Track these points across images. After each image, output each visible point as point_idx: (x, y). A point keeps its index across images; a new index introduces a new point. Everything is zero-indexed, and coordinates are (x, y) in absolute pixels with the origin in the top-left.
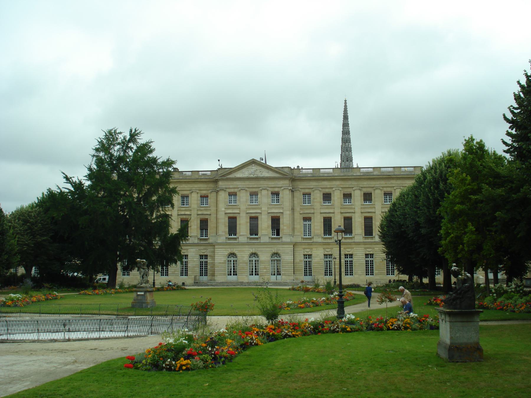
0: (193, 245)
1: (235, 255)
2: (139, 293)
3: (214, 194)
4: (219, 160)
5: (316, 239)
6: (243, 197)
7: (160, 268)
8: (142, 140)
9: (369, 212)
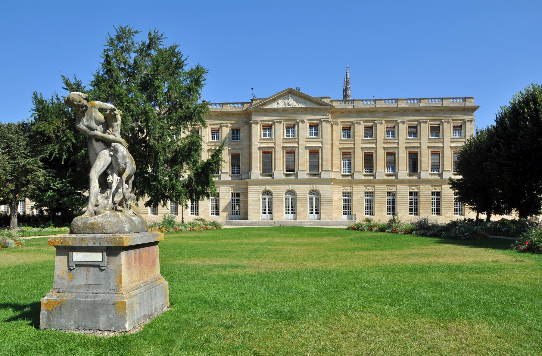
0: (226, 183)
1: (270, 192)
2: (77, 257)
3: (246, 128)
4: (252, 89)
5: (357, 176)
6: (280, 130)
7: (189, 203)
8: (164, 45)
9: (414, 147)
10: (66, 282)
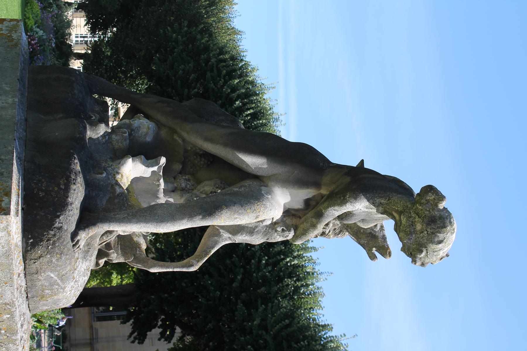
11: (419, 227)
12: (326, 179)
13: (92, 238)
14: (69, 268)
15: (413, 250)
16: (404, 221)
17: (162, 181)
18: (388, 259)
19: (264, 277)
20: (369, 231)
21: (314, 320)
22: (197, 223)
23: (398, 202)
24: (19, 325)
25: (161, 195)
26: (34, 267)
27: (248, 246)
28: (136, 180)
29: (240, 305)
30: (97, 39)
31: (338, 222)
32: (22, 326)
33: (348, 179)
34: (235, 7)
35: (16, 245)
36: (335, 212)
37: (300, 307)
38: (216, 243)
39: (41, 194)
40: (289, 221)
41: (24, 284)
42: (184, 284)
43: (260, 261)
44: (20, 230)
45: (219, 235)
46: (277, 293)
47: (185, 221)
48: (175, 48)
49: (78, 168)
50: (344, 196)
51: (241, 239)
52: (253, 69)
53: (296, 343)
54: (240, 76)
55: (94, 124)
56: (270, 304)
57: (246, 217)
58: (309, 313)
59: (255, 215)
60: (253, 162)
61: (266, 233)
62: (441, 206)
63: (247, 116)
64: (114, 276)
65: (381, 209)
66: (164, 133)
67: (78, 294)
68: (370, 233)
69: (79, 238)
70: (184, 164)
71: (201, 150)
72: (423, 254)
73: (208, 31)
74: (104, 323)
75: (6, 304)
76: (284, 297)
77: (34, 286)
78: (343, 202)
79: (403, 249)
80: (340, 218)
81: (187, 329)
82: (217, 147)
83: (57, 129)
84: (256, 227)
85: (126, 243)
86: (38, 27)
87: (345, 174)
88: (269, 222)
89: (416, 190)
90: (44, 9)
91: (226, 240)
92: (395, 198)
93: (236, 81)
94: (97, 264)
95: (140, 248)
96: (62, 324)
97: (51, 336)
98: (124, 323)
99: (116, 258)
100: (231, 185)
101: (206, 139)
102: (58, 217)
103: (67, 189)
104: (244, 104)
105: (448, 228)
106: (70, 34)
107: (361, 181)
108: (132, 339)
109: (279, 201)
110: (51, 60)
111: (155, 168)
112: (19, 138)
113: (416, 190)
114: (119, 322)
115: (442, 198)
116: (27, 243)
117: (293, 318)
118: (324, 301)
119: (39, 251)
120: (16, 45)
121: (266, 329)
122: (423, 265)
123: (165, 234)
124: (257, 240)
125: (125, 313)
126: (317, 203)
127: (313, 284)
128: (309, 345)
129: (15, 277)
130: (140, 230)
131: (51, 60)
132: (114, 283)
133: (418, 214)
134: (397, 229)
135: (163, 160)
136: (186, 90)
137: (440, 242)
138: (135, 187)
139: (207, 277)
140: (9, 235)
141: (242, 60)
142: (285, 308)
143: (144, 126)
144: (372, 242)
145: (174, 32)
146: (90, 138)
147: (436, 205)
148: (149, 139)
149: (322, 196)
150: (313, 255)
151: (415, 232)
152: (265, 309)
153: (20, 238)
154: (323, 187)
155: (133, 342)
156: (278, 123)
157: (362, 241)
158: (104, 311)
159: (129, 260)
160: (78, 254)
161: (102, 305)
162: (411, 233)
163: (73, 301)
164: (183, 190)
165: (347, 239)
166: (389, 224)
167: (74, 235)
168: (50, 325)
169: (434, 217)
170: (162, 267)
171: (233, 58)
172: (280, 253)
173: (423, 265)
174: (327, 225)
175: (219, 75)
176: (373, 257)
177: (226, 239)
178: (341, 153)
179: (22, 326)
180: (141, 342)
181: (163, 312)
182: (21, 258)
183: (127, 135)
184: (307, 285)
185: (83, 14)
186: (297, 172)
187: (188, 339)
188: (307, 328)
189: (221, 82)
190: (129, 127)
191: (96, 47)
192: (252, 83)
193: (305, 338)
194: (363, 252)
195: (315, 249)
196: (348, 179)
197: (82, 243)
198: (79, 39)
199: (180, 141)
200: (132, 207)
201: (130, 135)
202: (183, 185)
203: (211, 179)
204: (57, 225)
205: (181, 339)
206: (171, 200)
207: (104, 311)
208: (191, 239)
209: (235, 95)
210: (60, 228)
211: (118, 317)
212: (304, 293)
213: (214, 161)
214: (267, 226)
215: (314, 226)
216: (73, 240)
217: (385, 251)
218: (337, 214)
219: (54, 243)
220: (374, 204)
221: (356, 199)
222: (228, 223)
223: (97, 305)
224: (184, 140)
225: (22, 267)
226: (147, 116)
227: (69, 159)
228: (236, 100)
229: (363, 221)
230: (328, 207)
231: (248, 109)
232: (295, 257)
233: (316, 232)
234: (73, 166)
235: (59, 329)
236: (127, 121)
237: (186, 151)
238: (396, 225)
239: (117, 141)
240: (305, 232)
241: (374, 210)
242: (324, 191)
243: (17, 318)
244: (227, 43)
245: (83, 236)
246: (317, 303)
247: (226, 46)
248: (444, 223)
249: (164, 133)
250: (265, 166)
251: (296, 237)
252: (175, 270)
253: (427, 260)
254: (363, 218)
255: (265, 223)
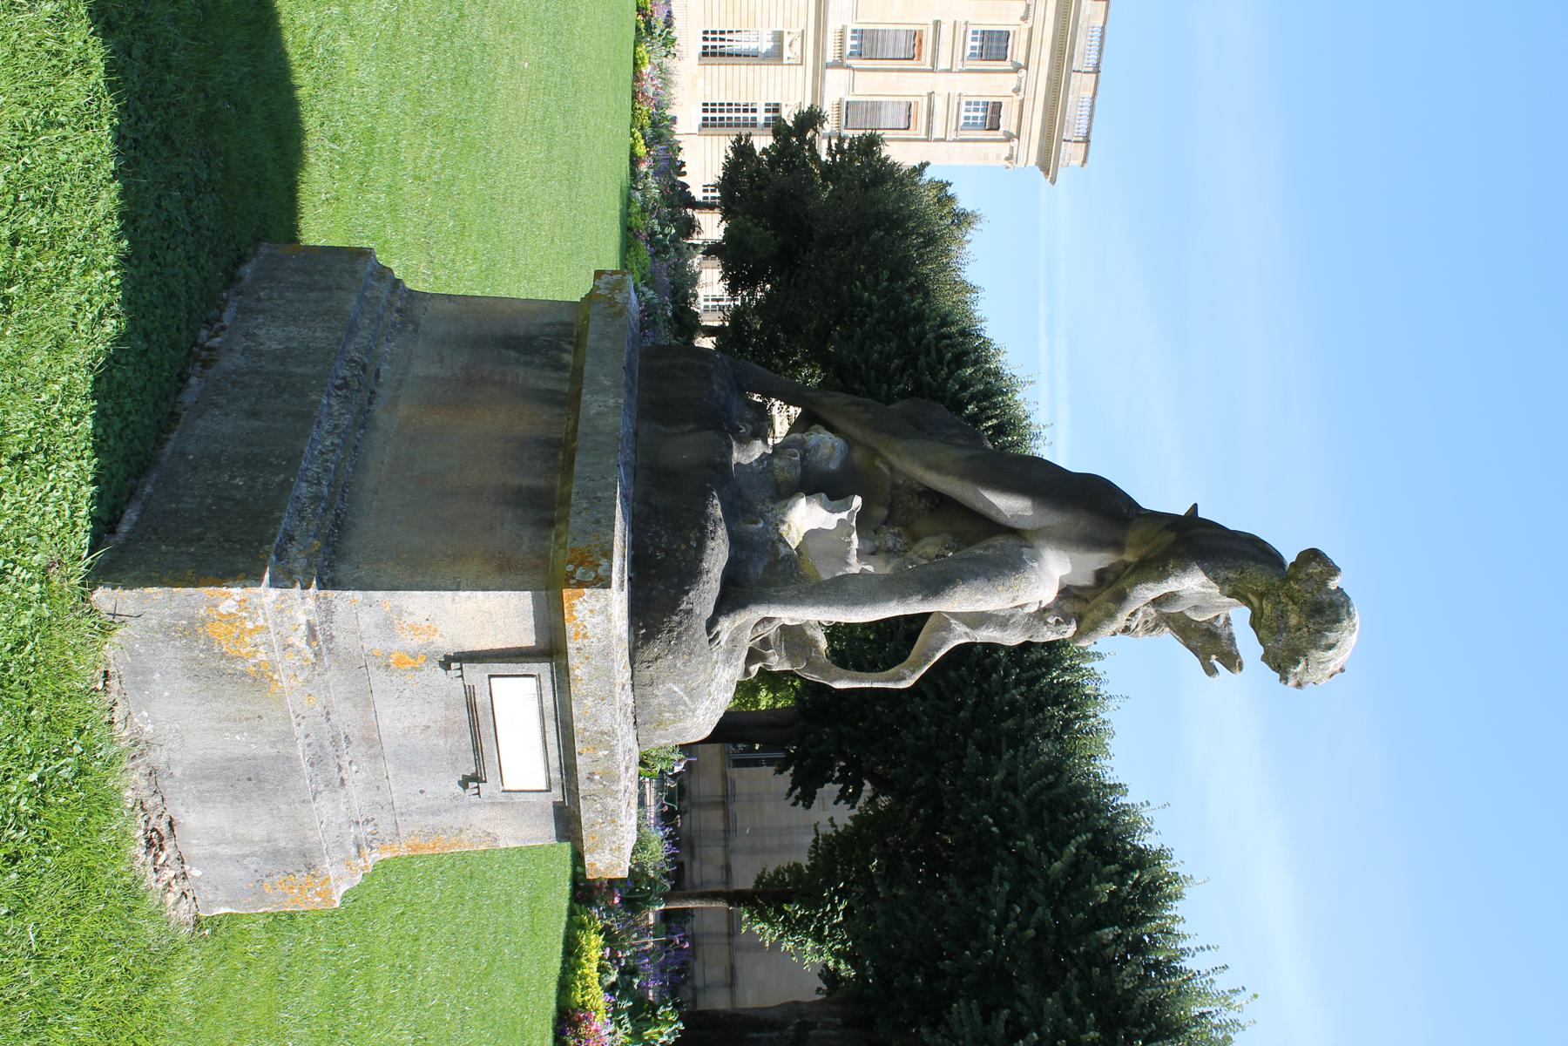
10: (374, 643)
11: (1293, 620)
12: (1133, 536)
13: (740, 629)
14: (702, 677)
15: (1282, 660)
16: (1267, 608)
17: (854, 536)
18: (1238, 675)
19: (1013, 702)
20: (1205, 626)
21: (1096, 776)
22: (914, 607)
23: (1259, 577)
24: (622, 769)
25: (853, 559)
26: (646, 674)
27: (991, 647)
28: (811, 534)
29: (971, 748)
30: (738, 303)
31: (1152, 610)
32: (627, 768)
33: (1171, 537)
34: (968, 247)
35: (620, 639)
36: (1149, 591)
37: (1072, 754)
38: (944, 642)
39: (660, 555)
40: (1068, 607)
41: (630, 701)
42: (879, 709)
43: (1007, 674)
44: (625, 614)
45: (947, 628)
46: (1033, 729)
47: (893, 604)
48: (866, 316)
49: (719, 513)
50: (1165, 566)
51: (985, 635)
52: (998, 351)
53: (1066, 814)
54: (976, 362)
55: (745, 441)
56: (1022, 748)
57: (996, 599)
58: (1088, 764)
59: (1011, 596)
60: (1009, 506)
61: (1028, 627)
62: (1333, 584)
63: (987, 429)
64: (763, 693)
65: (1227, 588)
66: (858, 456)
67: (716, 720)
68: (1208, 630)
69: (719, 628)
70: (891, 508)
71: (920, 484)
72: (1301, 666)
73: (922, 287)
74: (746, 770)
75: (602, 733)
76: (1046, 736)
77: (646, 705)
78: (1162, 576)
79: (1265, 658)
80: (1156, 602)
81: (881, 786)
82: (948, 479)
83: (685, 448)
84: (1012, 616)
85: (794, 638)
86: (646, 285)
87: (1168, 528)
88: (1033, 609)
89: (1290, 557)
90: (655, 254)
91: (960, 637)
92: (1253, 570)
93: (969, 371)
94: (747, 672)
95: (817, 647)
96: (677, 769)
97: (660, 787)
98: (780, 771)
99: (778, 662)
100: (969, 544)
101: (930, 467)
102: (687, 593)
103: (701, 548)
104: (982, 410)
105: (1345, 623)
106: (696, 296)
107: (1193, 540)
108: (792, 799)
109: (1053, 571)
110: (666, 337)
111: (844, 515)
112: (625, 464)
113: (1290, 557)
114: (772, 769)
115: (1334, 570)
116: (636, 635)
117: (1062, 773)
118: (1113, 745)
119: (655, 649)
120: (620, 313)
121: (1014, 789)
122: (1299, 685)
123: (847, 625)
124: (1012, 638)
125: (782, 755)
126: (1118, 577)
127: (1095, 716)
128: (1087, 817)
129: (618, 690)
130: (815, 617)
131: (666, 337)
132: (763, 706)
133: (1292, 598)
134: (1255, 623)
135: (857, 501)
136: (885, 387)
137: (1330, 647)
138: (809, 544)
139: (917, 700)
140: (610, 621)
141: (979, 336)
142: (1048, 754)
143: (827, 445)
144: (1210, 645)
145: (865, 288)
146: (738, 464)
147: (1325, 584)
148: (833, 466)
149: (1126, 565)
150: (1097, 665)
151: (1287, 628)
152: (1015, 757)
153: (626, 627)
154: (1128, 550)
155: (795, 804)
156: (1039, 442)
157: (1194, 644)
158: (745, 751)
159: (800, 668)
160: (717, 654)
161: (741, 741)
162: (1280, 631)
163: (709, 732)
164: (889, 551)
165: (1167, 639)
166: (1239, 616)
167: (712, 623)
168: (661, 771)
169: (1321, 603)
170: (852, 679)
171: (964, 333)
172: (1042, 662)
173: (1299, 685)
174: (1133, 614)
175: (940, 362)
176: (1211, 671)
177: (960, 636)
178: (1159, 490)
179: (627, 768)
180: (808, 806)
181: (843, 756)
182: (627, 658)
183: (797, 458)
184: (1086, 717)
185: (717, 262)
186: (1083, 523)
187: (884, 801)
188: (1085, 790)
189: (944, 372)
190: (801, 444)
191: (737, 316)
192: (997, 374)
193: (1080, 805)
194: (1193, 661)
195: (1099, 656)
196: (1171, 537)
197: (724, 637)
198: (710, 304)
199: (885, 470)
200: (805, 578)
201: (803, 458)
202: (890, 544)
203: (935, 535)
204: (683, 606)
205: (872, 801)
206: (870, 568)
207: (745, 751)
208: (897, 638)
209: (966, 394)
210: (689, 612)
211: (770, 762)
212: (1080, 730)
213: (941, 503)
214: (1030, 615)
215: (1111, 616)
216: (709, 632)
217: (1232, 660)
218: (1152, 596)
219: (679, 637)
220: (1215, 580)
221: (1184, 570)
222: (964, 609)
223: (735, 742)
224: (892, 468)
225: (628, 675)
226: (830, 428)
227: (705, 497)
228: (969, 403)
229: (1196, 608)
230: (1136, 584)
231: (990, 418)
232: (1065, 670)
233: (1114, 627)
234: (710, 510)
235: (674, 777)
236: (798, 436)
237: (895, 486)
238: (1253, 616)
239: (782, 469)
240: (1095, 627)
241: (1216, 590)
242: (1130, 557)
243: (620, 757)
244: (953, 308)
245: (726, 626)
246: (1102, 746)
247: (950, 313)
248: (1338, 615)
249: (858, 456)
250: (1030, 513)
251: (1079, 635)
252: (875, 685)
253: (1306, 678)
254: (1195, 603)
255: (1027, 610)
